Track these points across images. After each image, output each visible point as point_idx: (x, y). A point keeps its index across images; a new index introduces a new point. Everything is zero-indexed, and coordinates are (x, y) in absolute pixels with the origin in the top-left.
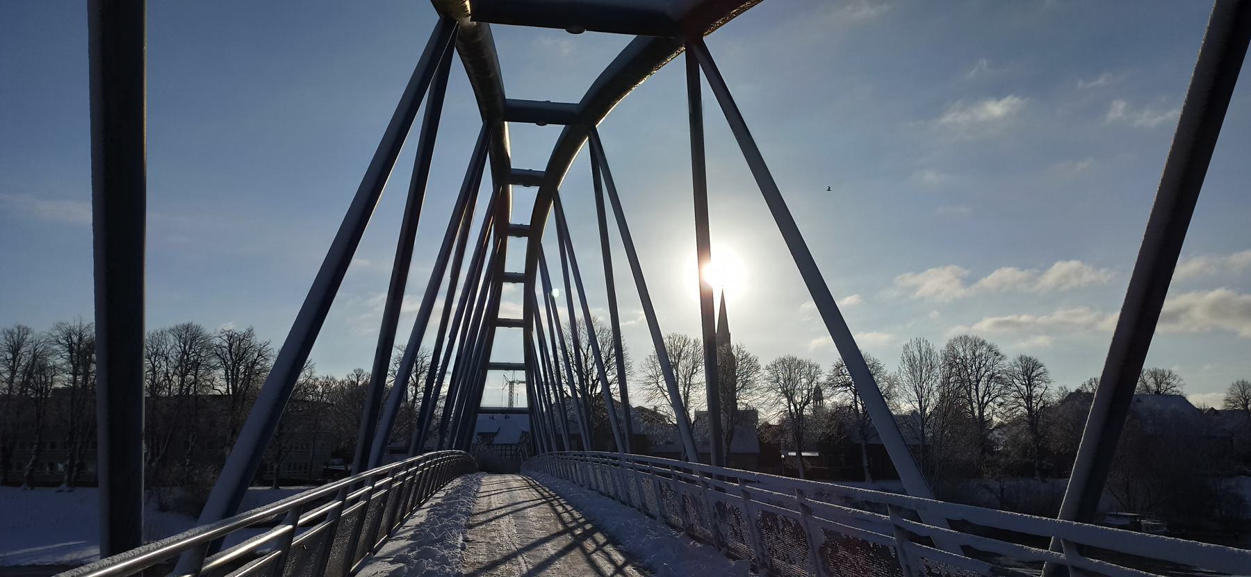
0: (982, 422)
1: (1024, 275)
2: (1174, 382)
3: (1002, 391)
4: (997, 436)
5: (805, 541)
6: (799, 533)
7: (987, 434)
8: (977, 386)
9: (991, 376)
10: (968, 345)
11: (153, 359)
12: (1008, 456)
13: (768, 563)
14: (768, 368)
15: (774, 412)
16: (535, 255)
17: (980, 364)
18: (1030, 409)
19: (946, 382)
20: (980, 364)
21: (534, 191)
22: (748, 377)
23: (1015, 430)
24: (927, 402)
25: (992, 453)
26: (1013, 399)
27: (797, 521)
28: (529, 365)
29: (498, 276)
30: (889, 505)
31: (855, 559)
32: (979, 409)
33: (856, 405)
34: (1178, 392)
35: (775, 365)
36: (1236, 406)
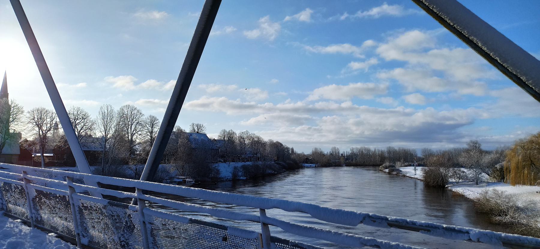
0: (132, 142)
1: (158, 83)
3: (141, 129)
4: (137, 147)
5: (26, 196)
6: (22, 192)
7: (133, 147)
8: (131, 127)
9: (138, 123)
10: (129, 109)
12: (140, 156)
13: (5, 208)
14: (29, 112)
15: (31, 133)
17: (133, 117)
18: (151, 137)
19: (118, 124)
20: (133, 117)
22: (17, 116)
23: (145, 145)
24: (109, 132)
25: (134, 154)
26: (145, 132)
27: (21, 186)
30: (67, 177)
31: (50, 202)
32: (131, 136)
34: (204, 132)
35: (33, 111)
36: (221, 138)
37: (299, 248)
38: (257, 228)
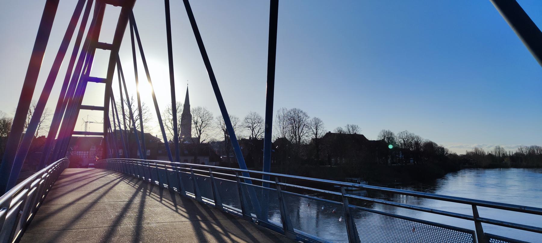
11: (202, 118)
33: (253, 135)
37: (507, 242)
38: (471, 225)
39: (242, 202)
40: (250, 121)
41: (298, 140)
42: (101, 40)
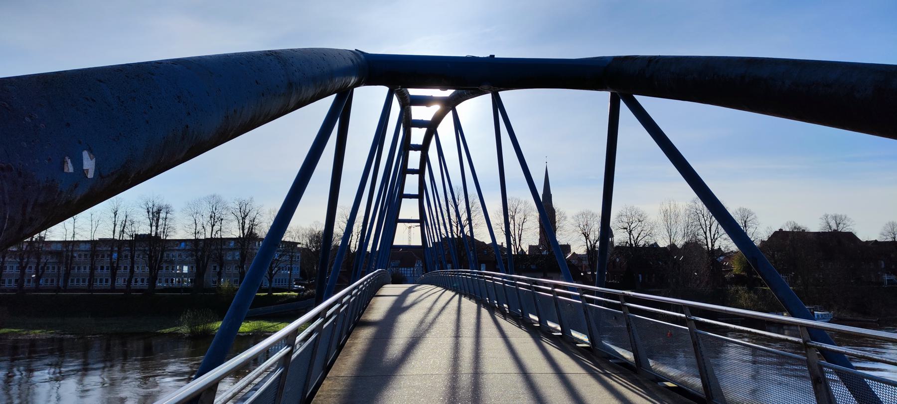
2: (848, 223)
8: (710, 228)
14: (573, 218)
16: (425, 159)
21: (424, 130)
28: (422, 220)
29: (405, 171)
34: (851, 229)
39: (537, 310)
40: (625, 219)
41: (710, 246)
42: (410, 167)
